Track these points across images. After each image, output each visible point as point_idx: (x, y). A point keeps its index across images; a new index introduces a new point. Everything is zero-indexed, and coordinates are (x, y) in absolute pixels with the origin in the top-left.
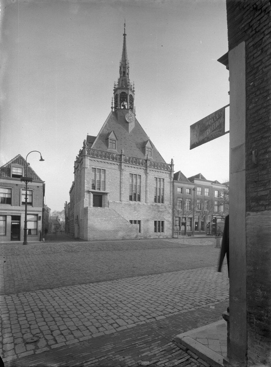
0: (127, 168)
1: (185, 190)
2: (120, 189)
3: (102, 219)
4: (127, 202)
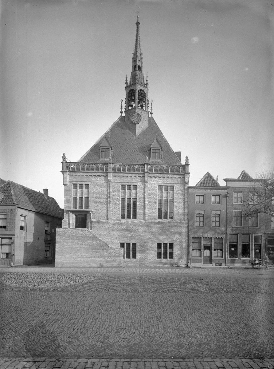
0: (117, 178)
1: (210, 199)
2: (107, 205)
3: (73, 242)
4: (117, 220)
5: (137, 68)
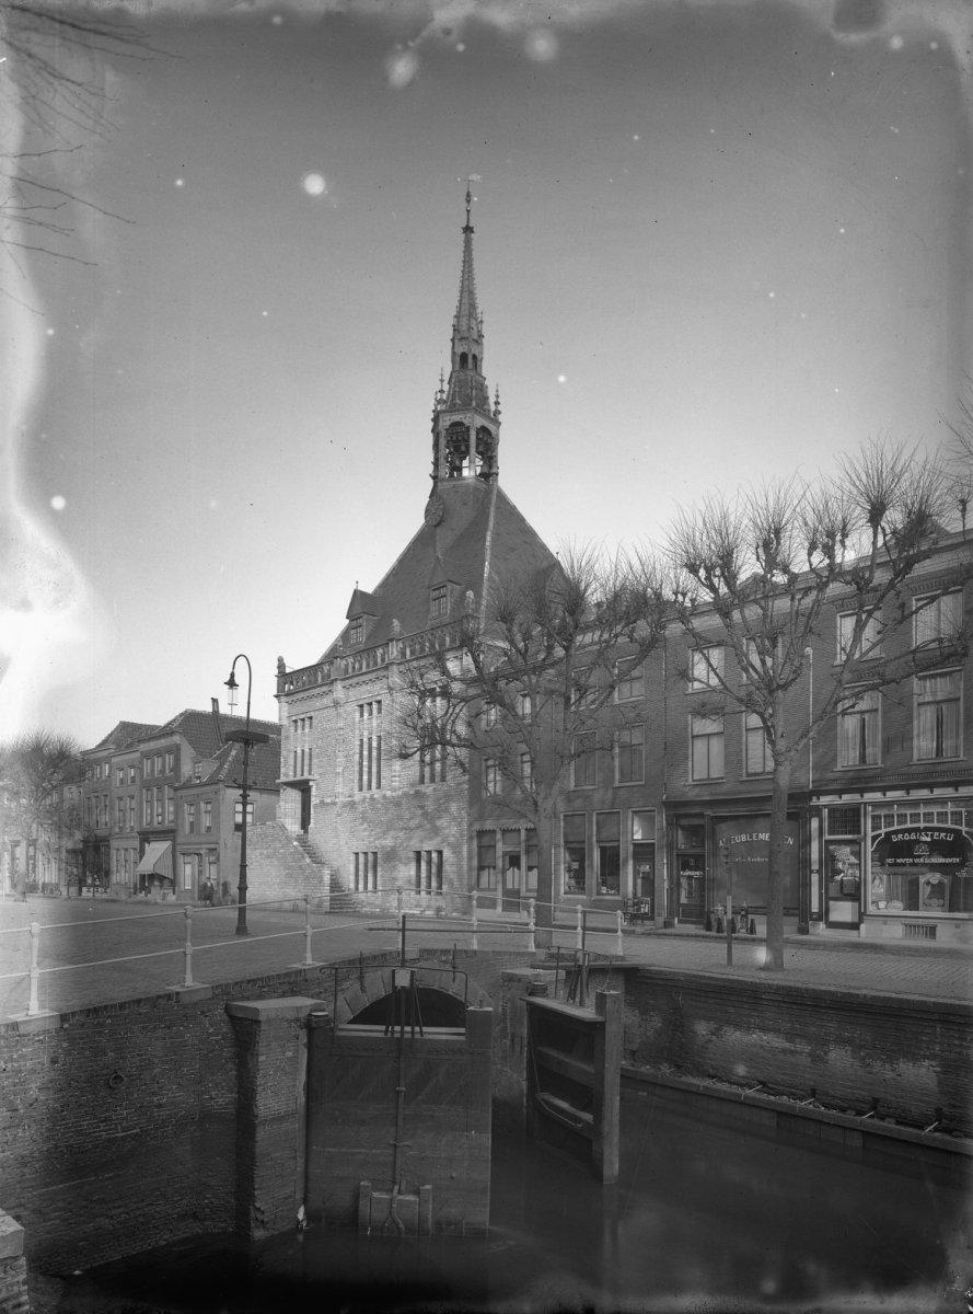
5: (466, 363)
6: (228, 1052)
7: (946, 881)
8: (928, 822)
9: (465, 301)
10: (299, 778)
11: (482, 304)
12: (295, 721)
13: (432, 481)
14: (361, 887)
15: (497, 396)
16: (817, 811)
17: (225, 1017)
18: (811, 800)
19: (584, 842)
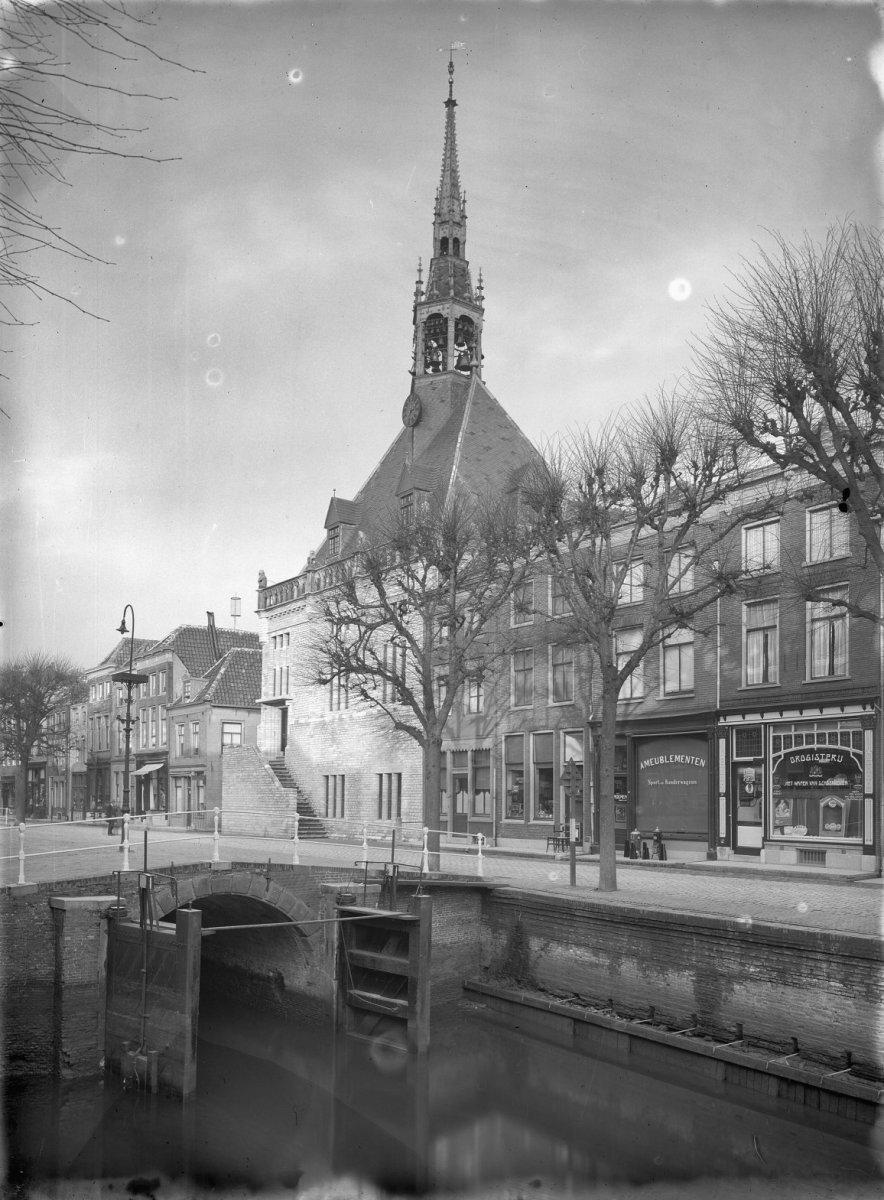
6: (48, 935)
7: (843, 804)
8: (821, 743)
9: (448, 180)
10: (280, 697)
11: (465, 183)
12: (275, 637)
13: (411, 377)
14: (330, 811)
15: (481, 281)
16: (725, 732)
17: (48, 908)
18: (719, 720)
19: (522, 764)
